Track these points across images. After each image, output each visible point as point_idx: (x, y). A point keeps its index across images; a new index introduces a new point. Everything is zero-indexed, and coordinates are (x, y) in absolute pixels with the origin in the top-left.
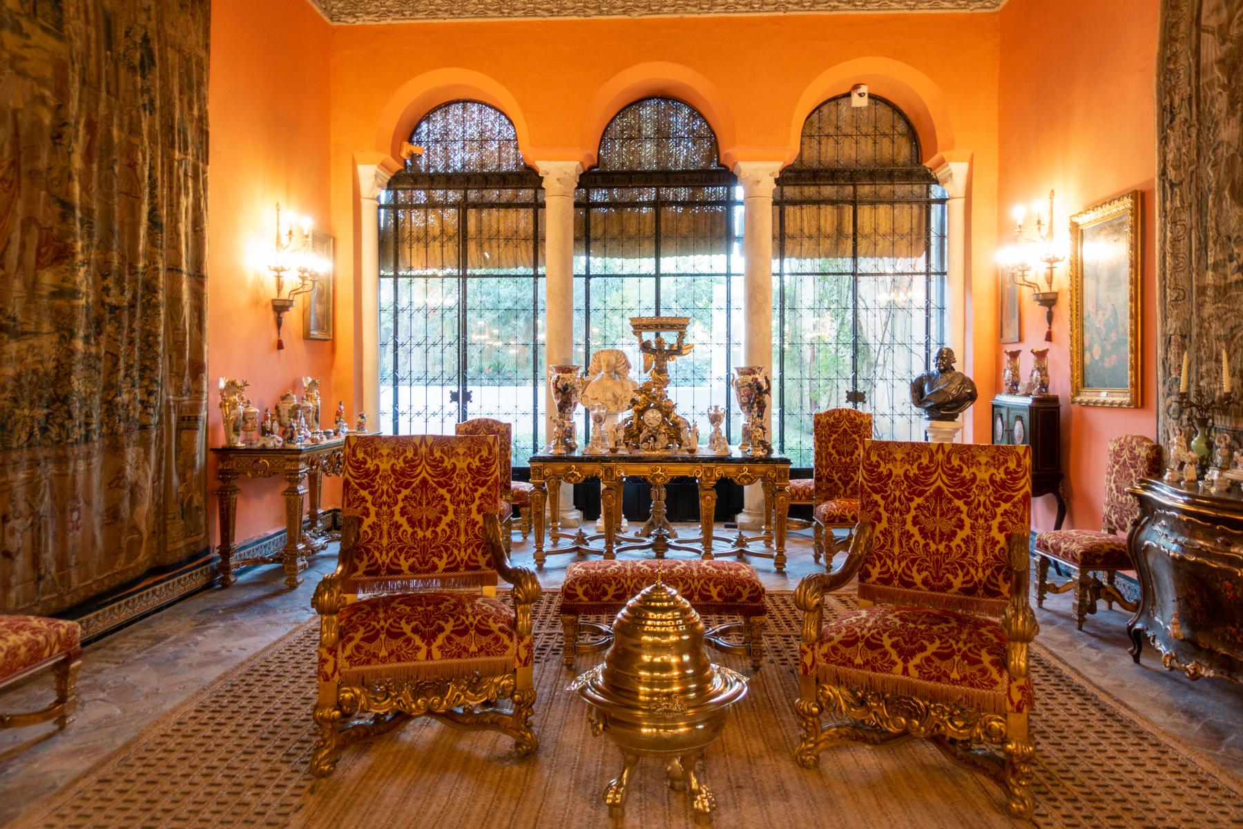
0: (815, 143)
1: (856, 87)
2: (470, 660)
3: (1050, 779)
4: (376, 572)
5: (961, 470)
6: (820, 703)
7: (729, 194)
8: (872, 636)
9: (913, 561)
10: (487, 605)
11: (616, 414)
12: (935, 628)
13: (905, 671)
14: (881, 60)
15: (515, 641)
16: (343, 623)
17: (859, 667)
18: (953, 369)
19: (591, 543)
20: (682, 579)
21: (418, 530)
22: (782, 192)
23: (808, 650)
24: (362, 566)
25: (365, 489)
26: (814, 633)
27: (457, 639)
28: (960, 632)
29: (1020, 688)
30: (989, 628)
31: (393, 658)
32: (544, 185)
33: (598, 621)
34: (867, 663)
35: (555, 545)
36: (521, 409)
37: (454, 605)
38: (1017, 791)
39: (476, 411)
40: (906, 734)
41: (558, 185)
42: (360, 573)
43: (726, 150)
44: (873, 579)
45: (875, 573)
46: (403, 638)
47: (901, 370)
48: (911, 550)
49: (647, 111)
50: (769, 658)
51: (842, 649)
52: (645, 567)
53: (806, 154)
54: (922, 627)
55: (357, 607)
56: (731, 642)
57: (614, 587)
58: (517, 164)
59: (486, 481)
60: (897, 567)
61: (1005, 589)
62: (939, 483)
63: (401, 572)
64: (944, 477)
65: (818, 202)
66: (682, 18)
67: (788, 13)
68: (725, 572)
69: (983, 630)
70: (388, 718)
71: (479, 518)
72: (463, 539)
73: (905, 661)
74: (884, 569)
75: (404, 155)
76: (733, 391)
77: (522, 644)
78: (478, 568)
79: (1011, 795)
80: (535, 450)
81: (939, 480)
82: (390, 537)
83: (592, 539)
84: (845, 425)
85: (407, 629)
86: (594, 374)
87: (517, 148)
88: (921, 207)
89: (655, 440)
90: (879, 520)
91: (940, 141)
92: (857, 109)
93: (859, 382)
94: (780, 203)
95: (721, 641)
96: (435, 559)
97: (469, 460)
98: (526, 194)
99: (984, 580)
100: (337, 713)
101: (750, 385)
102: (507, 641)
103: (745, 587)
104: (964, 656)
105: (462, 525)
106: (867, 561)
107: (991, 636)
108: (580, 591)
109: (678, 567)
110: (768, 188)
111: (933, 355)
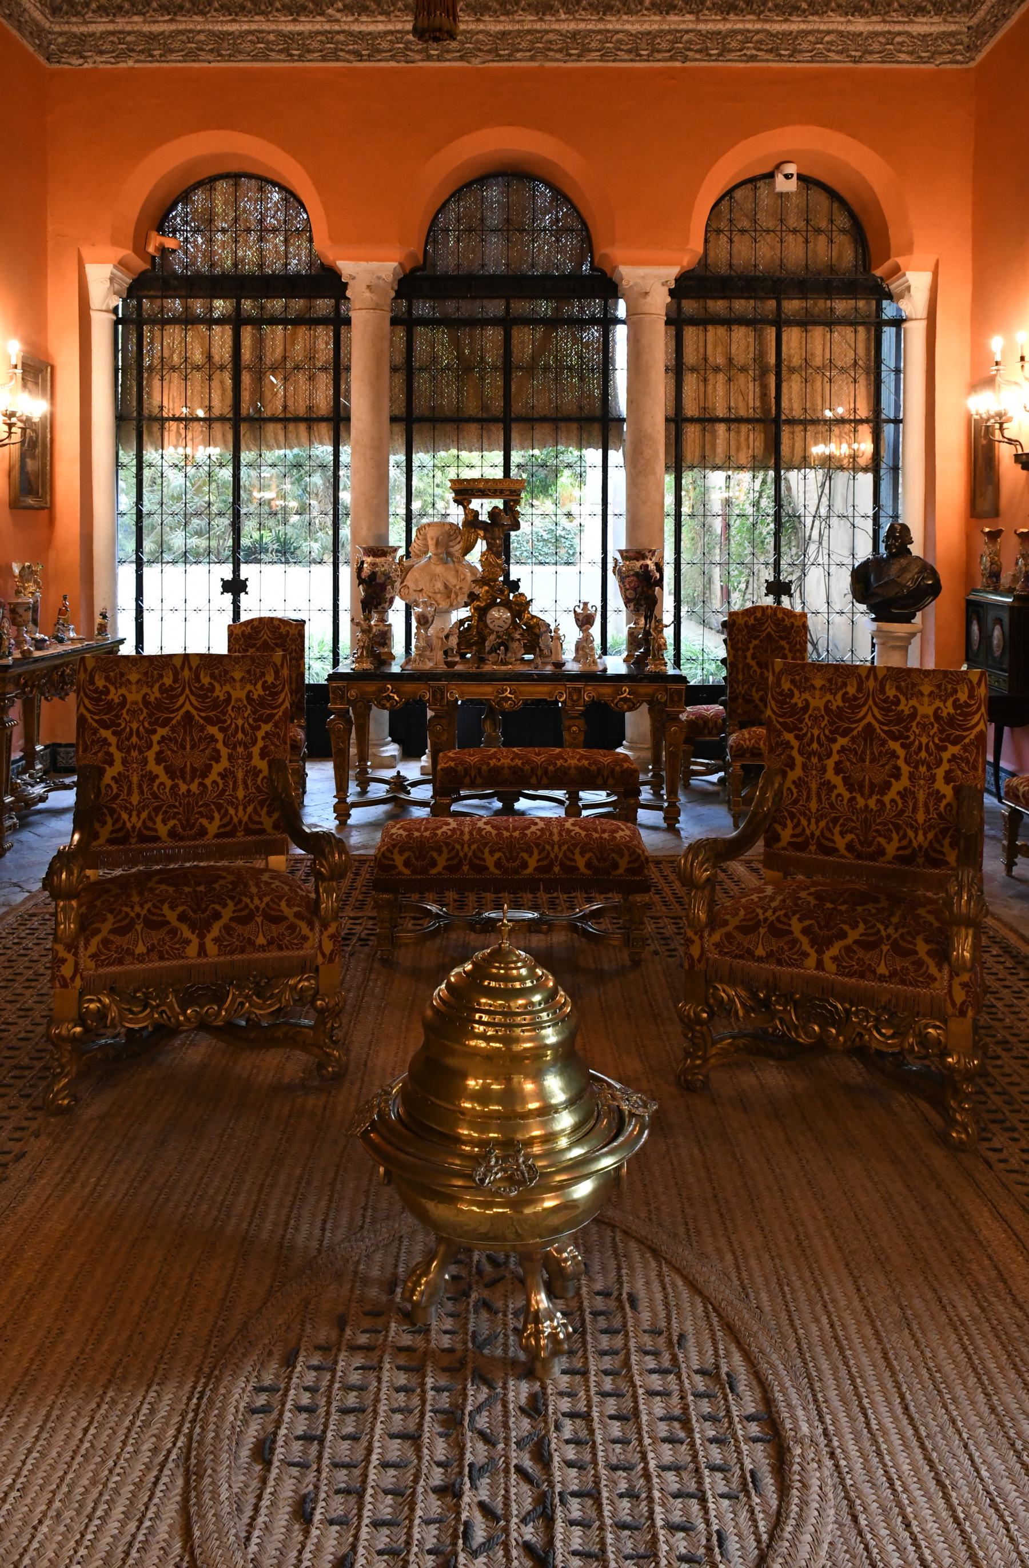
0: (724, 239)
1: (778, 167)
2: (256, 956)
3: (1009, 1103)
4: (124, 840)
5: (897, 702)
6: (710, 1007)
7: (605, 310)
8: (778, 919)
9: (835, 821)
10: (277, 883)
11: (448, 612)
12: (859, 909)
13: (820, 965)
14: (816, 130)
15: (317, 929)
16: (83, 910)
17: (760, 959)
18: (909, 552)
19: (413, 790)
20: (537, 845)
21: (180, 782)
22: (679, 308)
23: (696, 938)
24: (105, 833)
25: (107, 728)
26: (703, 916)
27: (239, 929)
28: (892, 914)
29: (964, 985)
30: (929, 908)
31: (154, 956)
32: (348, 294)
33: (422, 900)
34: (770, 954)
35: (364, 792)
36: (316, 604)
37: (233, 883)
38: (958, 1117)
39: (252, 608)
40: (820, 1046)
41: (368, 294)
42: (102, 840)
43: (603, 249)
44: (783, 843)
45: (786, 835)
46: (166, 929)
47: (841, 553)
48: (832, 806)
49: (494, 193)
50: (652, 948)
51: (739, 937)
52: (488, 828)
53: (711, 253)
54: (844, 908)
55: (99, 888)
56: (603, 927)
57: (445, 856)
58: (311, 264)
59: (271, 717)
60: (813, 828)
61: (952, 857)
62: (869, 719)
63: (157, 839)
64: (875, 710)
65: (728, 322)
66: (542, 67)
67: (688, 64)
68: (596, 835)
69: (921, 911)
70: (145, 1034)
71: (263, 765)
72: (240, 794)
73: (820, 952)
74: (798, 830)
75: (151, 249)
76: (612, 580)
77: (326, 934)
78: (262, 831)
79: (951, 1123)
80: (336, 663)
81: (187, 704)
82: (142, 792)
83: (415, 784)
84: (769, 628)
85: (171, 916)
86: (418, 556)
87: (311, 240)
88: (868, 331)
89: (507, 649)
90: (792, 766)
91: (893, 242)
92: (781, 195)
93: (784, 566)
94: (676, 321)
95: (591, 928)
96: (204, 821)
97: (249, 687)
98: (323, 305)
99: (926, 845)
100: (78, 1029)
101: (637, 574)
102: (305, 930)
103: (622, 855)
104: (896, 947)
105: (240, 775)
106: (775, 820)
107: (931, 918)
108: (399, 860)
109: (533, 828)
110: (659, 301)
111: (883, 533)
